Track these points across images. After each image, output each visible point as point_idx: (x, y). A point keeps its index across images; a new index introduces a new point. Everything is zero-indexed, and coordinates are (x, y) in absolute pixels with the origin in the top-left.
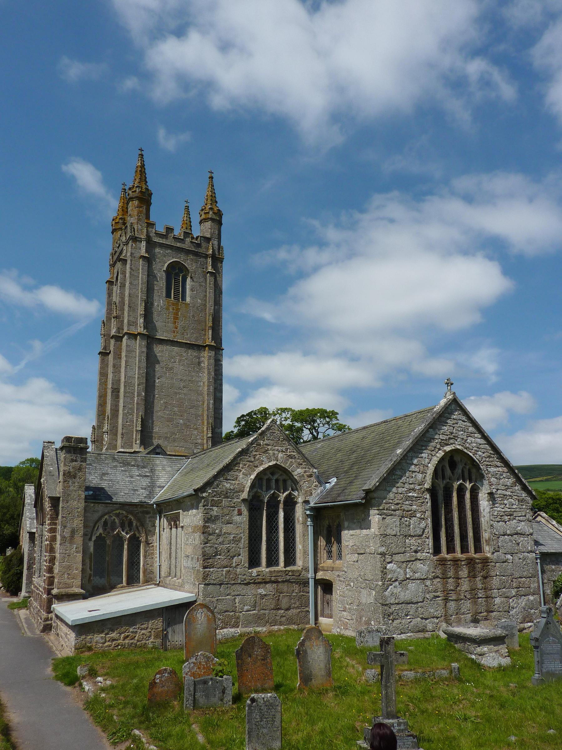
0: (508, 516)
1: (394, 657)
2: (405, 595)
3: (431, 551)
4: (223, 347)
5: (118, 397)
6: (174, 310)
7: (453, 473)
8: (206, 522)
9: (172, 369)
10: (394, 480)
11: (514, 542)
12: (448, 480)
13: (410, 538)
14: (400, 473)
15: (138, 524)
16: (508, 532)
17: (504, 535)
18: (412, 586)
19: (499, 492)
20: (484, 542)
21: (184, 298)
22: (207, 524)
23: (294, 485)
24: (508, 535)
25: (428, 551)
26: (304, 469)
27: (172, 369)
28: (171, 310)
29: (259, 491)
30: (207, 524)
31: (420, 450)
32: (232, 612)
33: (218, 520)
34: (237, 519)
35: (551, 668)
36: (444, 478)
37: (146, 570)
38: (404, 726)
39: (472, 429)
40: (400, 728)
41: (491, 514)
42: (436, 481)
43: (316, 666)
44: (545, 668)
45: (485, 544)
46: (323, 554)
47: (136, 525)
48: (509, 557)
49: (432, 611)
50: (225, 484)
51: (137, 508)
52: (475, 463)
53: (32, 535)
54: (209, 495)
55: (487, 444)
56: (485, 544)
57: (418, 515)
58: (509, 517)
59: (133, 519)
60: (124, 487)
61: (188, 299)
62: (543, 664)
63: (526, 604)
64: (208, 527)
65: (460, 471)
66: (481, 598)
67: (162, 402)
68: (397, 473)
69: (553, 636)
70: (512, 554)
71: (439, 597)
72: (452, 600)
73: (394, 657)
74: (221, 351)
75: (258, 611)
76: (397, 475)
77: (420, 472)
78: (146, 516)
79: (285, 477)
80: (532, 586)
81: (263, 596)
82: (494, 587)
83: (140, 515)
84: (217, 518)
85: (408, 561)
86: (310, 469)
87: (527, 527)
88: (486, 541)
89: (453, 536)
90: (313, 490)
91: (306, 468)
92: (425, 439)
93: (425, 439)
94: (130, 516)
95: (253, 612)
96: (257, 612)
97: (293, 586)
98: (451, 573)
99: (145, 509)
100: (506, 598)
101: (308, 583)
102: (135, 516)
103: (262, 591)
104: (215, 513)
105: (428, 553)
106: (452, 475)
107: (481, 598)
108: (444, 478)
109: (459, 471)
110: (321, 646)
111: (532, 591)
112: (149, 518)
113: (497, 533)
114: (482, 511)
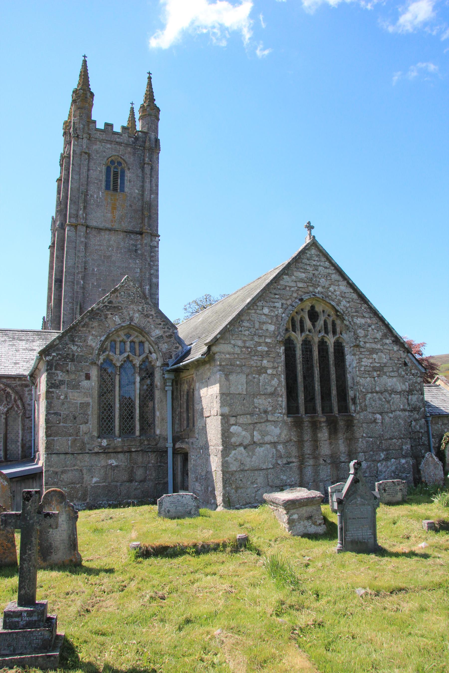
0: (378, 371)
1: (36, 518)
2: (251, 461)
3: (284, 411)
4: (159, 233)
5: (61, 286)
6: (112, 200)
7: (314, 325)
8: (51, 387)
9: (110, 257)
10: (240, 332)
11: (384, 400)
12: (307, 333)
13: (258, 397)
14: (248, 324)
15: (17, 398)
16: (377, 389)
17: (372, 393)
18: (260, 451)
19: (368, 345)
20: (350, 401)
21: (122, 190)
22: (51, 390)
23: (151, 347)
24: (377, 392)
25: (280, 411)
26: (163, 330)
27: (110, 257)
28: (109, 201)
29: (111, 354)
30: (51, 390)
31: (273, 298)
32: (78, 484)
33: (63, 384)
34: (85, 383)
35: (357, 536)
36: (302, 331)
37: (25, 445)
38: (38, 616)
39: (335, 277)
40: (31, 619)
41: (357, 369)
42: (293, 333)
43: (58, 537)
44: (350, 536)
45: (351, 403)
46: (183, 422)
47: (15, 397)
48: (378, 416)
49: (285, 478)
50: (72, 347)
51: (15, 381)
52: (338, 313)
53: (88, 377)
54: (53, 358)
55: (354, 293)
56: (351, 403)
57: (269, 371)
58: (378, 373)
59: (11, 392)
60: (5, 361)
61: (126, 190)
62: (347, 531)
63: (396, 468)
64: (52, 392)
65: (322, 322)
66: (343, 462)
67: (100, 290)
68: (244, 324)
69: (362, 497)
70: (381, 414)
71: (293, 462)
72: (309, 466)
73: (36, 518)
74: (157, 238)
75: (109, 483)
76: (244, 326)
77: (273, 324)
78: (25, 389)
79: (142, 338)
80: (404, 447)
81: (114, 468)
82: (359, 450)
83: (19, 388)
84: (62, 382)
85: (256, 423)
86: (170, 329)
87: (399, 383)
88: (352, 399)
89: (314, 394)
90: (173, 352)
91: (165, 328)
92: (279, 287)
93: (279, 287)
94: (8, 390)
95: (103, 484)
96: (107, 484)
97: (149, 456)
98: (307, 437)
99: (24, 382)
100: (373, 461)
101: (166, 452)
102: (13, 389)
103: (114, 462)
104: (60, 378)
105: (280, 413)
106: (312, 328)
107: (343, 462)
108: (302, 331)
109: (320, 323)
110: (64, 513)
111: (403, 453)
112: (28, 391)
113: (364, 390)
114: (348, 366)
